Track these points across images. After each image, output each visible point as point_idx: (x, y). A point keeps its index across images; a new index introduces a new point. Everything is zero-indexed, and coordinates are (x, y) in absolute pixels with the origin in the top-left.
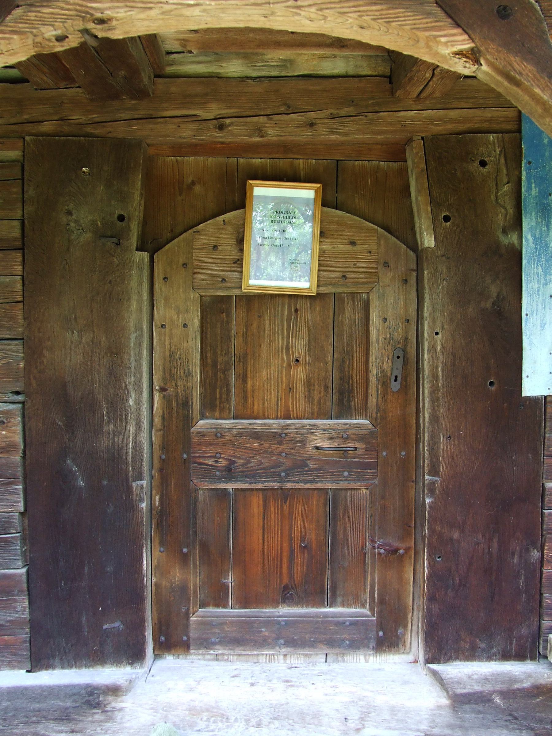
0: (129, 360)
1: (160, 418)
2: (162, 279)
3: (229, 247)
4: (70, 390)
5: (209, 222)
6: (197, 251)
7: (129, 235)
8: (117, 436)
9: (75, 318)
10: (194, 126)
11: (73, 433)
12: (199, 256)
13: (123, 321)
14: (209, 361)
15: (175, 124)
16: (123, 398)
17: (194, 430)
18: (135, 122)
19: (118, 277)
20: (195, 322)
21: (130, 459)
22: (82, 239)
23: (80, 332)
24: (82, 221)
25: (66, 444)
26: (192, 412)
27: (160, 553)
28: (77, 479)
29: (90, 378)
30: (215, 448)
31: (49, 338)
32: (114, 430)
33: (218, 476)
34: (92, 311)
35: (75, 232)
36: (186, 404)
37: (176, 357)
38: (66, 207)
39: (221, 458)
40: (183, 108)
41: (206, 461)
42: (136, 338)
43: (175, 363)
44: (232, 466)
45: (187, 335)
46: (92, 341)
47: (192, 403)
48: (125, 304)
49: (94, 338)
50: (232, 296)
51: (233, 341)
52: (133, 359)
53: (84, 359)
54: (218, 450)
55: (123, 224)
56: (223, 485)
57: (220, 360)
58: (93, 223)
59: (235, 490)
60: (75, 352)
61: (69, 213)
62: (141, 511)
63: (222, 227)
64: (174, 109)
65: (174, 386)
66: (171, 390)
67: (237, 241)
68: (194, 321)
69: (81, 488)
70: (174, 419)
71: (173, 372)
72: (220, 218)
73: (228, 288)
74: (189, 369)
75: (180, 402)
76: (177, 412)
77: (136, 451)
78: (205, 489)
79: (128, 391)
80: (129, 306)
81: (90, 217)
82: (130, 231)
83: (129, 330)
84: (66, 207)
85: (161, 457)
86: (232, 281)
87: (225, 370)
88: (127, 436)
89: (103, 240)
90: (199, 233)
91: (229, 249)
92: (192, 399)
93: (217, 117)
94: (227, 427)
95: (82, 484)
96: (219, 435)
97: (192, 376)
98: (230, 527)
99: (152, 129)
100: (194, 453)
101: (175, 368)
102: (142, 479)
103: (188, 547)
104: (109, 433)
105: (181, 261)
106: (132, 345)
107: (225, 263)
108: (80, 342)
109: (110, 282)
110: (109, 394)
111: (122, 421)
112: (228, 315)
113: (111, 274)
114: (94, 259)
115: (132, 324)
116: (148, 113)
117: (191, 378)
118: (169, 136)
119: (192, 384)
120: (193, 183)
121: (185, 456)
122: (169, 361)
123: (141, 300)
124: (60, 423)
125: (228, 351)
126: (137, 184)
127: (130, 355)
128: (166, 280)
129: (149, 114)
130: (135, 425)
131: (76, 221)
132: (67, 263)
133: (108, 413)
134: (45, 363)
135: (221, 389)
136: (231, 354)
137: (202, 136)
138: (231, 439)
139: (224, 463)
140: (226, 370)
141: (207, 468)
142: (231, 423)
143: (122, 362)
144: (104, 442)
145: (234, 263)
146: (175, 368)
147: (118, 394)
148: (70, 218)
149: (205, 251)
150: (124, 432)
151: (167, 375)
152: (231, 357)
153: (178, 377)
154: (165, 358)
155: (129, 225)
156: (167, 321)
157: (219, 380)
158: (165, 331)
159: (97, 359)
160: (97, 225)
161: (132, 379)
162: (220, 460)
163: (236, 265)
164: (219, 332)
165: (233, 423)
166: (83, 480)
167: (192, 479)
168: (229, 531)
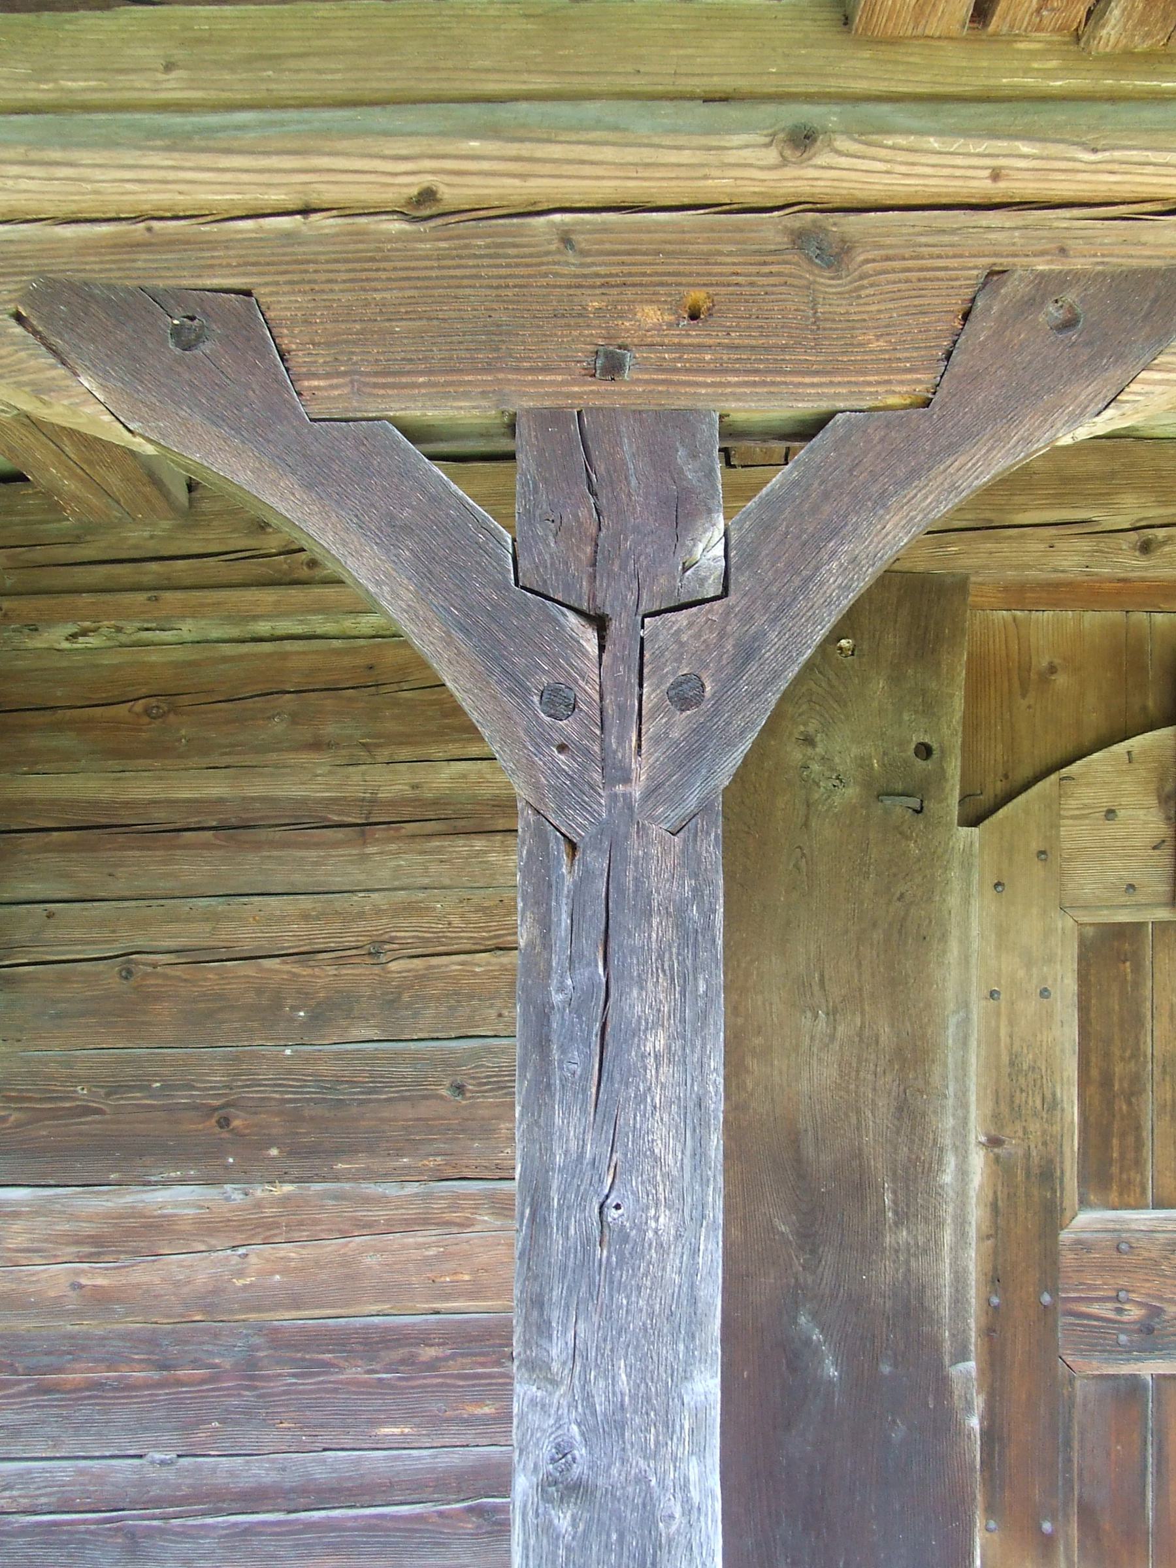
0: (944, 1077)
1: (988, 1209)
2: (991, 886)
3: (1141, 812)
4: (809, 1151)
5: (1095, 756)
6: (1071, 822)
7: (943, 790)
8: (915, 1255)
9: (822, 980)
10: (1085, 545)
11: (813, 1252)
12: (1073, 834)
13: (930, 988)
14: (1094, 1073)
15: (1042, 541)
16: (930, 1168)
17: (1065, 1236)
18: (953, 536)
19: (918, 886)
20: (1067, 984)
21: (946, 1312)
22: (837, 800)
23: (832, 1013)
24: (837, 760)
25: (797, 1280)
26: (1062, 1193)
27: (988, 1535)
28: (821, 1362)
29: (854, 1120)
30: (1114, 1277)
31: (760, 1027)
32: (909, 1244)
33: (1124, 1346)
34: (860, 965)
35: (821, 783)
36: (1047, 1175)
37: (1025, 1067)
38: (802, 728)
39: (1129, 1301)
40: (1061, 506)
41: (1095, 1309)
42: (958, 1025)
43: (1022, 1080)
44: (1157, 1320)
45: (1050, 1015)
46: (860, 1035)
47: (1062, 1173)
48: (935, 947)
49: (862, 1027)
50: (1147, 923)
51: (1149, 1027)
52: (951, 1076)
53: (841, 1077)
54: (1122, 1282)
55: (929, 765)
56: (1136, 1367)
57: (1118, 1069)
58: (862, 762)
59: (1159, 1379)
60: (820, 1060)
61: (809, 741)
62: (969, 1438)
63: (1124, 767)
64: (1038, 508)
65: (1020, 1134)
66: (1012, 1147)
67: (1159, 797)
68: (1066, 981)
69: (830, 1382)
70: (1021, 1210)
71: (1017, 1102)
72: (1120, 748)
73: (1139, 906)
74: (1054, 1094)
75: (1036, 1171)
76: (1028, 1195)
77: (957, 1290)
78: (1087, 1377)
79: (941, 1149)
80: (944, 952)
81: (855, 751)
82: (947, 780)
83: (945, 1008)
84: (802, 728)
85: (988, 1301)
86: (1150, 890)
87: (1132, 1094)
88: (938, 1257)
89: (888, 801)
90: (1073, 782)
91: (1142, 817)
92: (1062, 1162)
93: (1138, 525)
94: (1143, 1228)
95: (833, 1372)
96: (1123, 1247)
97: (1063, 1110)
98: (1146, 1467)
99: (991, 553)
100: (1066, 1291)
101: (1022, 1091)
102: (968, 1360)
103: (1054, 1519)
104: (897, 1251)
105: (1035, 846)
106: (950, 1041)
107: (1134, 848)
108: (832, 1037)
109: (902, 896)
110: (898, 1158)
111: (926, 1221)
112: (1137, 968)
113: (904, 878)
114: (864, 845)
115: (950, 994)
116: (982, 516)
117: (1058, 1113)
118: (1030, 567)
119: (1062, 1128)
120: (1052, 669)
121: (1046, 1298)
122: (1010, 1075)
123: (967, 937)
124: (783, 1228)
125: (1138, 1049)
126: (959, 674)
127: (945, 1065)
128: (1000, 888)
129: (984, 520)
130: (955, 1230)
131: (823, 759)
132: (803, 855)
133: (895, 1202)
134: (750, 1085)
135: (1123, 1135)
136: (1145, 1056)
137: (1102, 566)
138: (1154, 1255)
139: (1138, 1312)
140: (1134, 1090)
141: (1095, 1327)
142: (1151, 1220)
143: (927, 1083)
144: (886, 1273)
145: (1155, 848)
146: (1022, 1091)
147: (918, 1158)
148: (810, 751)
149: (1087, 822)
150: (930, 1248)
151: (1004, 1108)
152: (1146, 1062)
153: (1029, 1112)
154: (998, 1068)
155: (942, 768)
156: (1003, 982)
157: (1118, 1117)
158: (999, 1007)
159: (870, 1077)
160: (872, 768)
161: (950, 1122)
162: (1127, 1307)
163: (1157, 852)
164: (1117, 1007)
165: (1158, 1219)
166: (836, 1364)
167: (1061, 1351)
168: (1143, 1475)
